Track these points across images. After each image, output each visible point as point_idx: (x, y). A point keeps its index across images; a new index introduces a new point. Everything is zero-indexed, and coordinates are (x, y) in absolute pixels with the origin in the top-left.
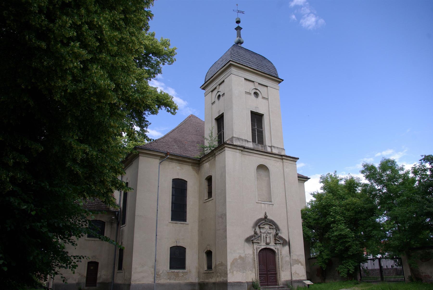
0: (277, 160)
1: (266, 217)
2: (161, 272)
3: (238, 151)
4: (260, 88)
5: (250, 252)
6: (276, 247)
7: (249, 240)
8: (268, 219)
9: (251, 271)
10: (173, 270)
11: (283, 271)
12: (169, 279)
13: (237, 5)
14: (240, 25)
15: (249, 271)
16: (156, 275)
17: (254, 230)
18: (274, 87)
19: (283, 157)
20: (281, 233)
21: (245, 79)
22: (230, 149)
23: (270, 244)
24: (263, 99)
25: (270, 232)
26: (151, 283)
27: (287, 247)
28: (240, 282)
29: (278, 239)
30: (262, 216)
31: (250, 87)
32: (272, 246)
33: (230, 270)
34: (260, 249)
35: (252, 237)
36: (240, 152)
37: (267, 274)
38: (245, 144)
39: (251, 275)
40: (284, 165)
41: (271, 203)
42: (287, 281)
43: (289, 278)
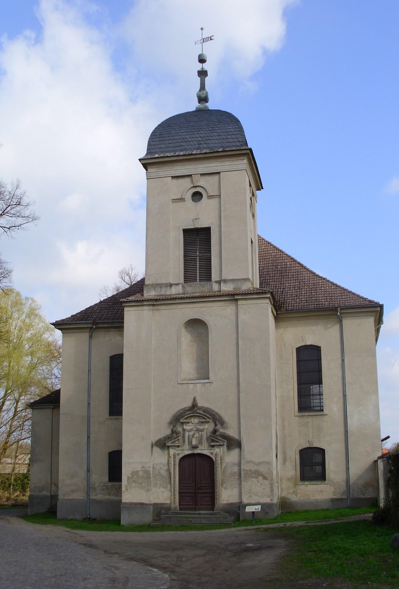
0: (222, 303)
1: (194, 405)
2: (97, 485)
3: (146, 308)
4: (202, 182)
5: (163, 463)
6: (212, 451)
7: (162, 444)
8: (200, 408)
9: (164, 487)
10: (114, 483)
11: (226, 489)
12: (109, 494)
13: (202, 29)
14: (206, 66)
15: (159, 488)
16: (89, 488)
17: (172, 427)
18: (235, 168)
19: (236, 297)
20: (225, 428)
21: (173, 177)
22: (132, 309)
23: (200, 447)
24: (209, 200)
25: (202, 427)
26: (82, 498)
27: (235, 452)
28: (142, 504)
29: (219, 438)
30: (189, 404)
31: (184, 187)
32: (204, 450)
33: (126, 486)
34: (181, 456)
35: (168, 438)
36: (151, 308)
37: (195, 493)
38: (166, 291)
39: (164, 494)
40: (239, 309)
41: (207, 381)
42: (231, 504)
43: (235, 500)
